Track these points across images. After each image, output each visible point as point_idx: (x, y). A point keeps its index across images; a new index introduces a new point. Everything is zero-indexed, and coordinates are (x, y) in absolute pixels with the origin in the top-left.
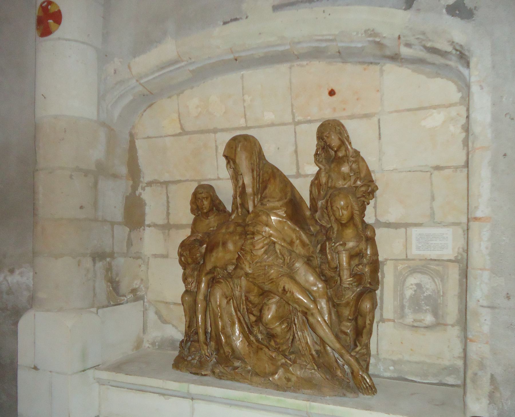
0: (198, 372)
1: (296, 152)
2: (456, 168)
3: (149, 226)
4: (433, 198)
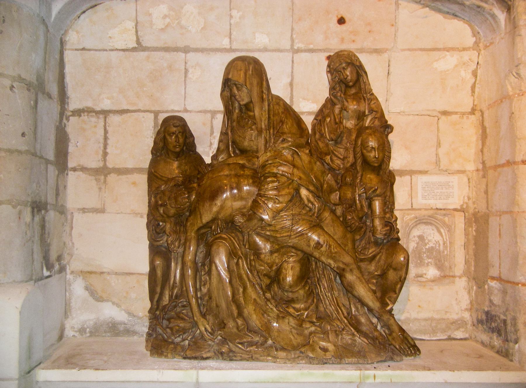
0: (198, 354)
1: (291, 84)
2: (463, 114)
3: (74, 169)
4: (439, 145)
